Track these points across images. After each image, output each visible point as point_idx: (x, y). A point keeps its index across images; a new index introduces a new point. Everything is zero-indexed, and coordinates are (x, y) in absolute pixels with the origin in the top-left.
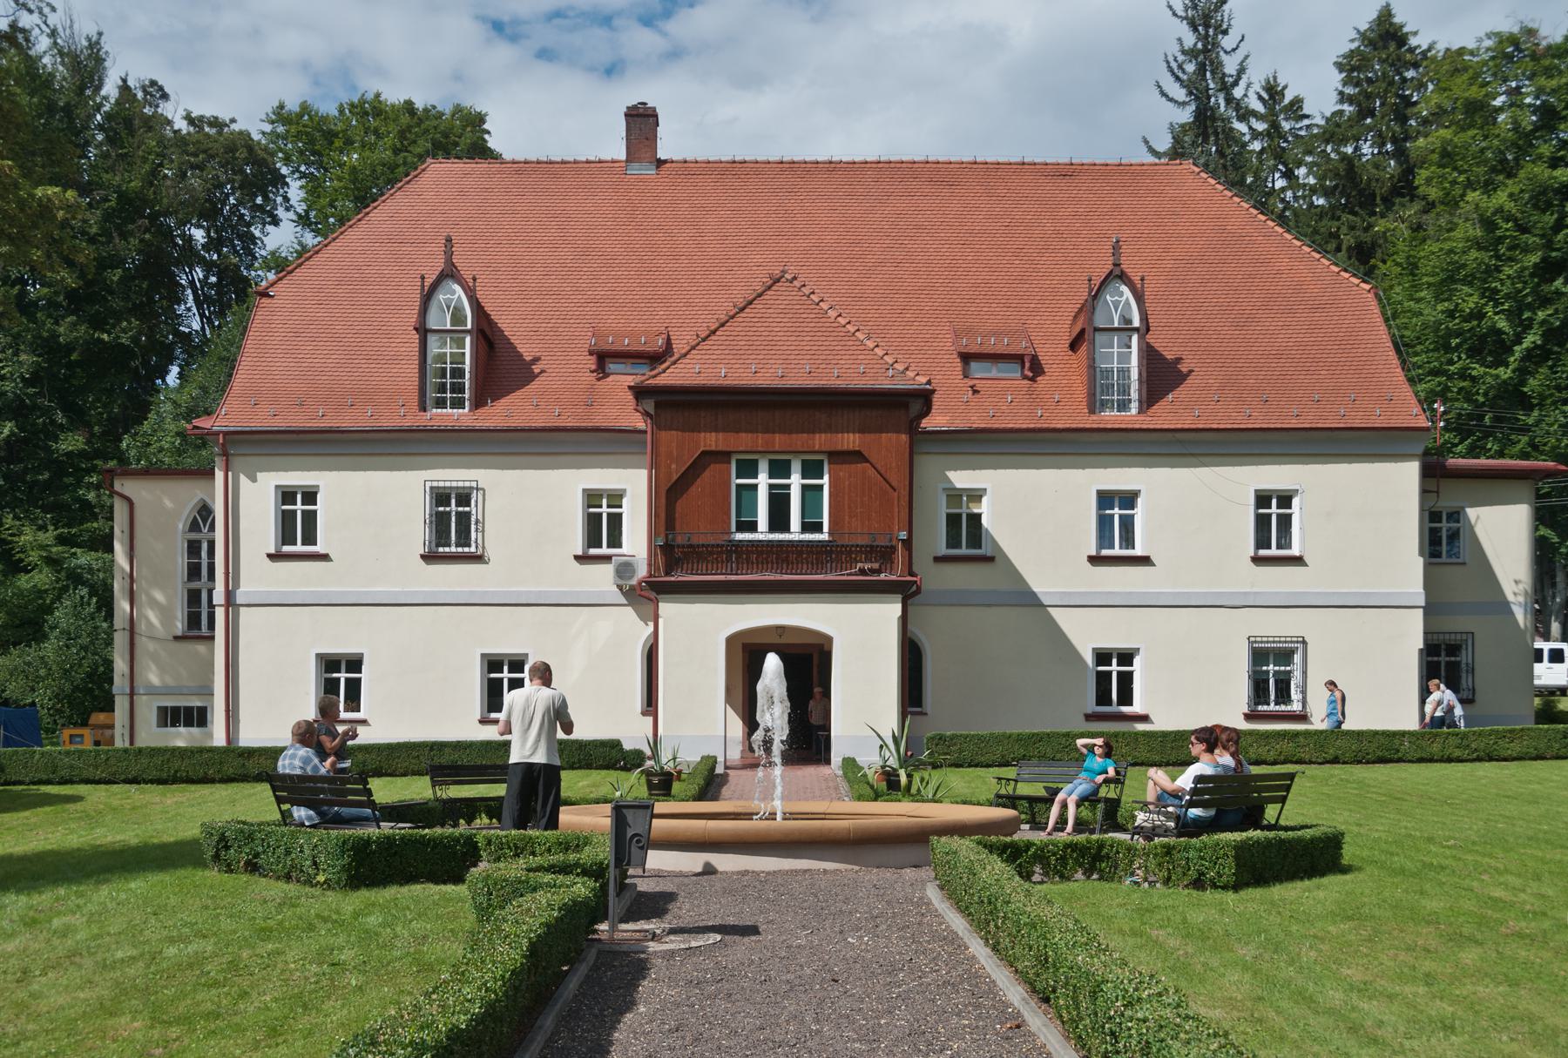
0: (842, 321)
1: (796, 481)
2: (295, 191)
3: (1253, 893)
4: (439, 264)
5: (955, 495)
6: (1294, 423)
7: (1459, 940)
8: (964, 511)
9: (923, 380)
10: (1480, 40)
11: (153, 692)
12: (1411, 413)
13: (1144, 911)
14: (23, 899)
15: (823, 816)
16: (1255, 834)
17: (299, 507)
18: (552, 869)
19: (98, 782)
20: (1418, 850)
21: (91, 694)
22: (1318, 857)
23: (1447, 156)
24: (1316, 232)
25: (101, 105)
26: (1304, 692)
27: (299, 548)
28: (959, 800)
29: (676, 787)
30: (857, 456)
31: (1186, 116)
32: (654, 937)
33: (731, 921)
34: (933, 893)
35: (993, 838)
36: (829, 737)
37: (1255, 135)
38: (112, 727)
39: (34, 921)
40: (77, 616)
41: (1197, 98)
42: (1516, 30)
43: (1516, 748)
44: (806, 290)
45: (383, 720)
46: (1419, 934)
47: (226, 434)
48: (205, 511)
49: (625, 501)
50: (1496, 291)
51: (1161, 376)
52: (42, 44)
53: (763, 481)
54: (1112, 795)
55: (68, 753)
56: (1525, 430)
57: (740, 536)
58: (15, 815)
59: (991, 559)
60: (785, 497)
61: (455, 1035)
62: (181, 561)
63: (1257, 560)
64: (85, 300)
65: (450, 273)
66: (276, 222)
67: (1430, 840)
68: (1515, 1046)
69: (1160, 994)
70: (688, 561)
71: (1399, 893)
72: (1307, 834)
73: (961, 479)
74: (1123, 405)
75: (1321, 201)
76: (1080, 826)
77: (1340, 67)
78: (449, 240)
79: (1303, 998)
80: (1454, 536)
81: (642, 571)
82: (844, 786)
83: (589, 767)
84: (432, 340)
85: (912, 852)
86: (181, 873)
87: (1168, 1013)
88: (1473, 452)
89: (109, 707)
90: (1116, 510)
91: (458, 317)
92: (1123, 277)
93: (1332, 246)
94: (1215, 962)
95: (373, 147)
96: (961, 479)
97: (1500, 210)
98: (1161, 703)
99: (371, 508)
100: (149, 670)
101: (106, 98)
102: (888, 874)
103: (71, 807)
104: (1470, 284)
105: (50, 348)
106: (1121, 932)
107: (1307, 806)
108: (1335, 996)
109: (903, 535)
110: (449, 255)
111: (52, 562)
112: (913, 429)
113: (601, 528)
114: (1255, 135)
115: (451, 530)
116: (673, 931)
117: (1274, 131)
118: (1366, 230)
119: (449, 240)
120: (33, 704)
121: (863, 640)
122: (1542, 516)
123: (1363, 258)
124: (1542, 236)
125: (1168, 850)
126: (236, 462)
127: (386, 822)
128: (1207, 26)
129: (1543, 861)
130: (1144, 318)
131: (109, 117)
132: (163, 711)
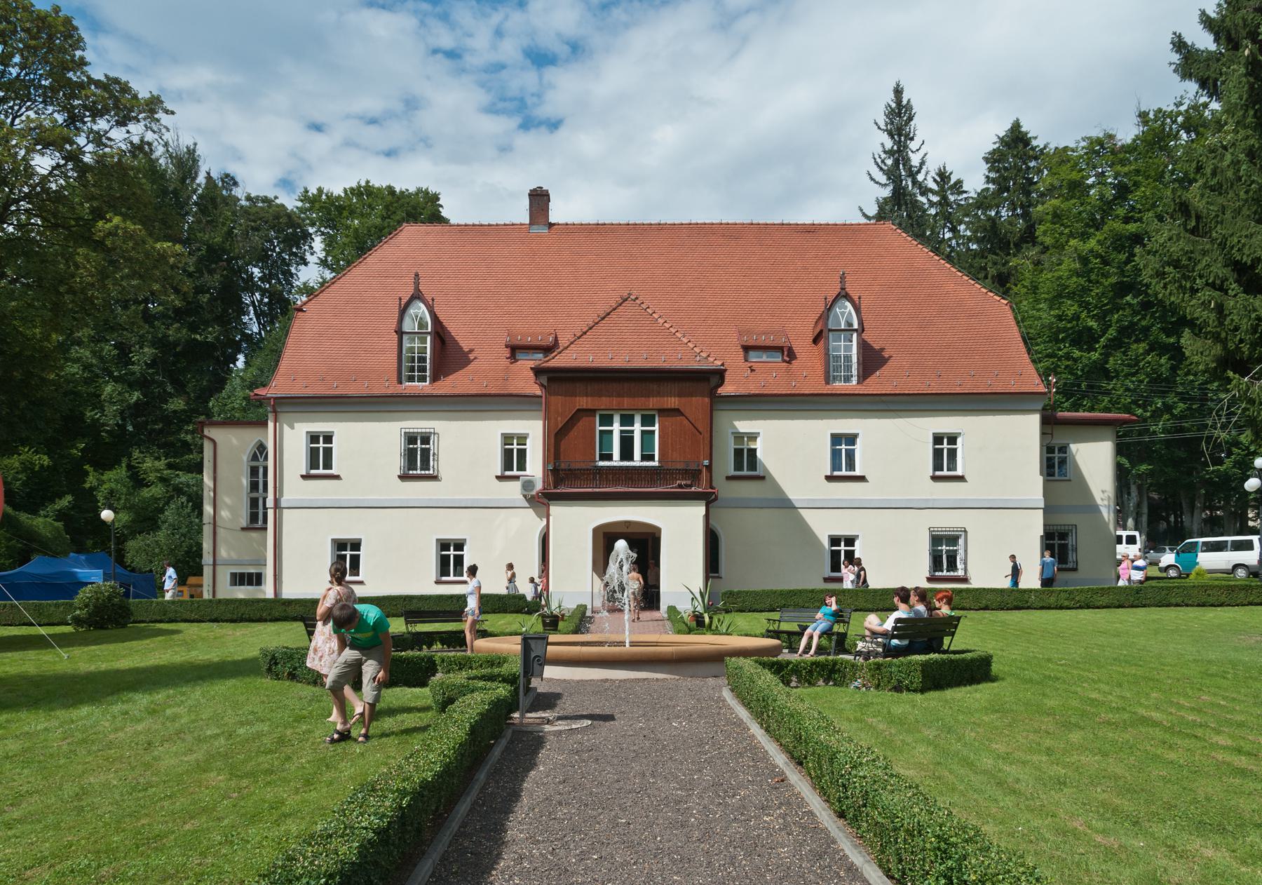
1: (637, 428)
2: (318, 244)
5: (739, 437)
6: (958, 390)
7: (1068, 726)
8: (745, 447)
9: (719, 363)
10: (1078, 142)
12: (1032, 381)
15: (656, 644)
18: (483, 678)
22: (976, 671)
23: (1057, 216)
24: (971, 266)
25: (195, 191)
26: (965, 564)
27: (321, 471)
28: (743, 634)
29: (561, 625)
30: (676, 412)
31: (887, 192)
32: (549, 722)
33: (598, 711)
34: (727, 694)
37: (932, 204)
38: (201, 586)
39: (154, 711)
42: (1101, 135)
43: (1105, 600)
44: (644, 306)
46: (1042, 722)
47: (275, 398)
48: (262, 448)
49: (528, 441)
50: (1088, 303)
51: (871, 360)
52: (159, 151)
53: (616, 428)
54: (841, 630)
56: (1107, 393)
57: (601, 464)
60: (630, 438)
61: (424, 785)
62: (245, 482)
63: (934, 478)
65: (417, 296)
67: (1049, 660)
68: (1105, 796)
69: (874, 760)
70: (569, 480)
72: (969, 656)
73: (743, 426)
74: (848, 379)
75: (975, 247)
76: (821, 650)
77: (986, 160)
78: (417, 275)
80: (1063, 462)
81: (539, 486)
83: (505, 612)
84: (405, 337)
85: (713, 668)
86: (248, 680)
88: (1076, 407)
91: (422, 325)
92: (847, 297)
93: (981, 275)
94: (909, 739)
96: (743, 426)
97: (1091, 251)
99: (367, 445)
100: (225, 548)
101: (199, 185)
102: (697, 681)
103: (175, 637)
104: (1072, 299)
105: (162, 344)
106: (849, 720)
107: (968, 638)
108: (987, 762)
109: (706, 462)
110: (417, 284)
111: (163, 480)
112: (713, 395)
113: (513, 458)
115: (418, 459)
116: (560, 718)
117: (944, 202)
118: (1004, 265)
119: (417, 275)
120: (151, 571)
121: (680, 528)
122: (1120, 450)
123: (1002, 283)
124: (1118, 268)
125: (878, 667)
126: (282, 417)
127: (408, 642)
128: (900, 135)
131: (200, 197)
132: (234, 575)
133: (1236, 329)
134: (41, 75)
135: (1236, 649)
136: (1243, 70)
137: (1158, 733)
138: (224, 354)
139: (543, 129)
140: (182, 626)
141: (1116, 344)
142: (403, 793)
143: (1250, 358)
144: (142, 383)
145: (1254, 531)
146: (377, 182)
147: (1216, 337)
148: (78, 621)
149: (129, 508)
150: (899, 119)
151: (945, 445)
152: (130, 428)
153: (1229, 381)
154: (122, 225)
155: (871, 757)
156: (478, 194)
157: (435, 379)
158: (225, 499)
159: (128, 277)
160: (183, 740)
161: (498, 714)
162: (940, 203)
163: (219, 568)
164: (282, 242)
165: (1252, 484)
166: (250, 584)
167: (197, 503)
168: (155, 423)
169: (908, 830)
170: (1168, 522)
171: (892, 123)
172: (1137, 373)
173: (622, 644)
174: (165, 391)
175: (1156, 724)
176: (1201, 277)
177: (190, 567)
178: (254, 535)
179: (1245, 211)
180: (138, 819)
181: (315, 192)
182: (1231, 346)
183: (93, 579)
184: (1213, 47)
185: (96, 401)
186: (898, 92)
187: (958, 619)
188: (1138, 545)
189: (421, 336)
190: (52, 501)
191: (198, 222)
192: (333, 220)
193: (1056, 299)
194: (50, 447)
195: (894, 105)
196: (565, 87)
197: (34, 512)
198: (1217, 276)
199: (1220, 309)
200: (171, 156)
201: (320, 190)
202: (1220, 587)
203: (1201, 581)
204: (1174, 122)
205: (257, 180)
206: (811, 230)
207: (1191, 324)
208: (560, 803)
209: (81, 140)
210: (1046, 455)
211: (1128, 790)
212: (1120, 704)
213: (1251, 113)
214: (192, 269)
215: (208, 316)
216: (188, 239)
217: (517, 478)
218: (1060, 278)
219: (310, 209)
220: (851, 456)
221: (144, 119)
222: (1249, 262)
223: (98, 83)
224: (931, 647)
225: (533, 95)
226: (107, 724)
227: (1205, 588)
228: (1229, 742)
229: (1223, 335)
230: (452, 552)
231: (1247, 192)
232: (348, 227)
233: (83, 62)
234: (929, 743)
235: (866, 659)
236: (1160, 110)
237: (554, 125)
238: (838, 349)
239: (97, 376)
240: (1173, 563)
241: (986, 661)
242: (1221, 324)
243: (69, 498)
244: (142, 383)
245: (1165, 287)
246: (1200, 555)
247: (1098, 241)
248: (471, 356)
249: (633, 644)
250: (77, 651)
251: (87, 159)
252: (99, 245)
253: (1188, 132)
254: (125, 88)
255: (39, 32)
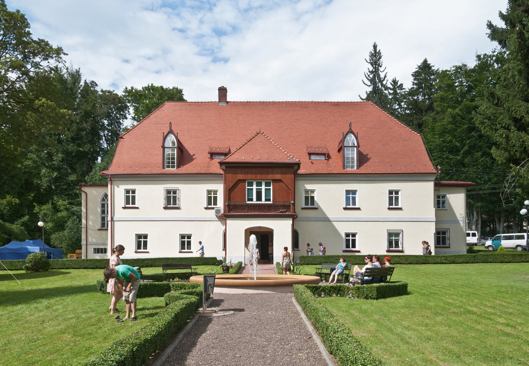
0: (276, 144)
1: (263, 187)
2: (132, 110)
3: (382, 300)
4: (168, 129)
5: (307, 191)
6: (399, 172)
7: (436, 314)
8: (309, 195)
9: (298, 160)
10: (451, 68)
11: (92, 244)
12: (430, 168)
13: (350, 305)
14: (48, 301)
15: (268, 279)
16: (382, 284)
17: (131, 195)
18: (187, 293)
19: (76, 268)
20: (430, 288)
21: (76, 245)
22: (401, 290)
23: (442, 99)
24: (407, 120)
25: (80, 88)
26: (402, 245)
27: (131, 206)
28: (307, 274)
29: (231, 270)
30: (280, 181)
31: (370, 89)
32: (215, 312)
33: (238, 307)
34: (294, 300)
35: (310, 285)
36: (273, 257)
37: (390, 94)
38: (81, 254)
39: (49, 307)
40: (73, 223)
41: (373, 84)
42: (461, 65)
43: (460, 260)
44: (266, 136)
45: (154, 251)
46: (426, 312)
47: (111, 175)
48: (106, 196)
49: (218, 193)
50: (456, 135)
51: (362, 159)
52: (65, 71)
53: (255, 187)
54: (347, 273)
55: (68, 261)
56: (464, 173)
57: (248, 202)
58: (53, 277)
59: (317, 209)
60: (260, 192)
61: (146, 341)
62: (99, 210)
63: (389, 209)
64: (76, 139)
65: (171, 132)
66: (126, 118)
67: (434, 286)
68: (447, 345)
69: (344, 330)
70: (235, 209)
71: (422, 301)
72: (397, 284)
73: (309, 187)
74: (352, 167)
75: (408, 112)
76: (339, 281)
77: (413, 75)
78: (171, 123)
79: (390, 330)
80: (444, 203)
81: (222, 212)
82: (276, 270)
83: (208, 264)
84: (166, 150)
85: (289, 289)
86: (91, 294)
87: (345, 335)
88: (450, 179)
89: (81, 249)
90: (351, 195)
91: (173, 143)
92: (352, 132)
93: (411, 124)
94: (367, 319)
95: (152, 98)
96: (309, 187)
97: (457, 113)
98: (363, 247)
99: (151, 194)
100: (91, 238)
101: (81, 86)
102: (283, 295)
103: (68, 275)
104: (449, 134)
105: (67, 153)
106: (343, 311)
107: (398, 276)
108: (399, 330)
109: (292, 202)
110: (171, 127)
111: (67, 209)
112: (295, 174)
113: (211, 200)
114: (390, 94)
115: (171, 201)
116: (221, 310)
117: (395, 93)
118: (420, 119)
119: (171, 123)
120: (62, 247)
121: (282, 230)
122: (468, 197)
123: (419, 127)
124: (468, 121)
125: (358, 288)
126: (113, 182)
127: (151, 280)
128: (376, 65)
129: (464, 292)
130: (358, 143)
131: (82, 90)
132: (95, 249)
133: (514, 146)
134: (12, 39)
135: (514, 281)
136: (516, 36)
137: (474, 317)
138: (92, 156)
139: (222, 62)
140: (71, 270)
141: (468, 153)
142: (134, 345)
143: (520, 158)
144: (58, 169)
145: (525, 231)
146: (157, 84)
147: (506, 150)
148: (27, 268)
149: (53, 221)
150: (375, 58)
151: (394, 195)
152: (54, 187)
153: (511, 168)
154: (46, 102)
155: (343, 328)
156: (199, 90)
157: (178, 167)
158: (90, 217)
159: (48, 124)
160: (58, 320)
161: (191, 310)
162: (393, 93)
163: (88, 246)
164: (117, 109)
165: (523, 211)
166: (102, 253)
167: (80, 218)
168: (63, 185)
169: (351, 361)
170: (525, 226)
171: (372, 60)
172: (477, 165)
173: (252, 278)
174: (67, 172)
175: (474, 313)
176: (499, 124)
177: (78, 246)
178: (104, 232)
179: (518, 96)
180: (28, 355)
181: (130, 89)
182: (512, 153)
183: (35, 251)
184: (504, 27)
185: (38, 175)
186: (375, 47)
187: (394, 268)
188: (477, 237)
189: (172, 148)
190: (20, 218)
191: (81, 101)
192: (138, 100)
193: (441, 135)
194: (20, 195)
195: (373, 52)
196: (230, 45)
197: (12, 222)
198: (506, 124)
199: (507, 137)
200: (69, 74)
201: (132, 88)
202: (509, 255)
203: (502, 252)
204: (492, 59)
205: (103, 85)
206: (337, 104)
207: (495, 144)
208: (213, 348)
209: (29, 66)
210: (436, 199)
211: (457, 342)
212: (461, 304)
213: (520, 54)
214: (78, 121)
215: (85, 141)
216: (77, 108)
217: (213, 208)
218: (443, 125)
219: (128, 96)
220: (354, 199)
221: (55, 57)
222: (519, 118)
223: (35, 42)
224: (382, 282)
225: (217, 48)
226: (27, 313)
227: (503, 255)
228: (504, 321)
229: (509, 148)
230: (186, 240)
231: (518, 88)
232: (144, 103)
233: (29, 34)
234: (375, 321)
235: (354, 285)
236: (485, 54)
237: (226, 60)
238: (348, 154)
239: (39, 165)
240: (491, 244)
241: (405, 286)
242: (508, 144)
243: (27, 217)
244: (58, 169)
245: (485, 128)
246: (502, 241)
247: (460, 109)
248: (194, 157)
249: (258, 278)
250: (25, 281)
251: (31, 74)
252: (36, 110)
253: (497, 64)
254: (47, 44)
255: (10, 21)
